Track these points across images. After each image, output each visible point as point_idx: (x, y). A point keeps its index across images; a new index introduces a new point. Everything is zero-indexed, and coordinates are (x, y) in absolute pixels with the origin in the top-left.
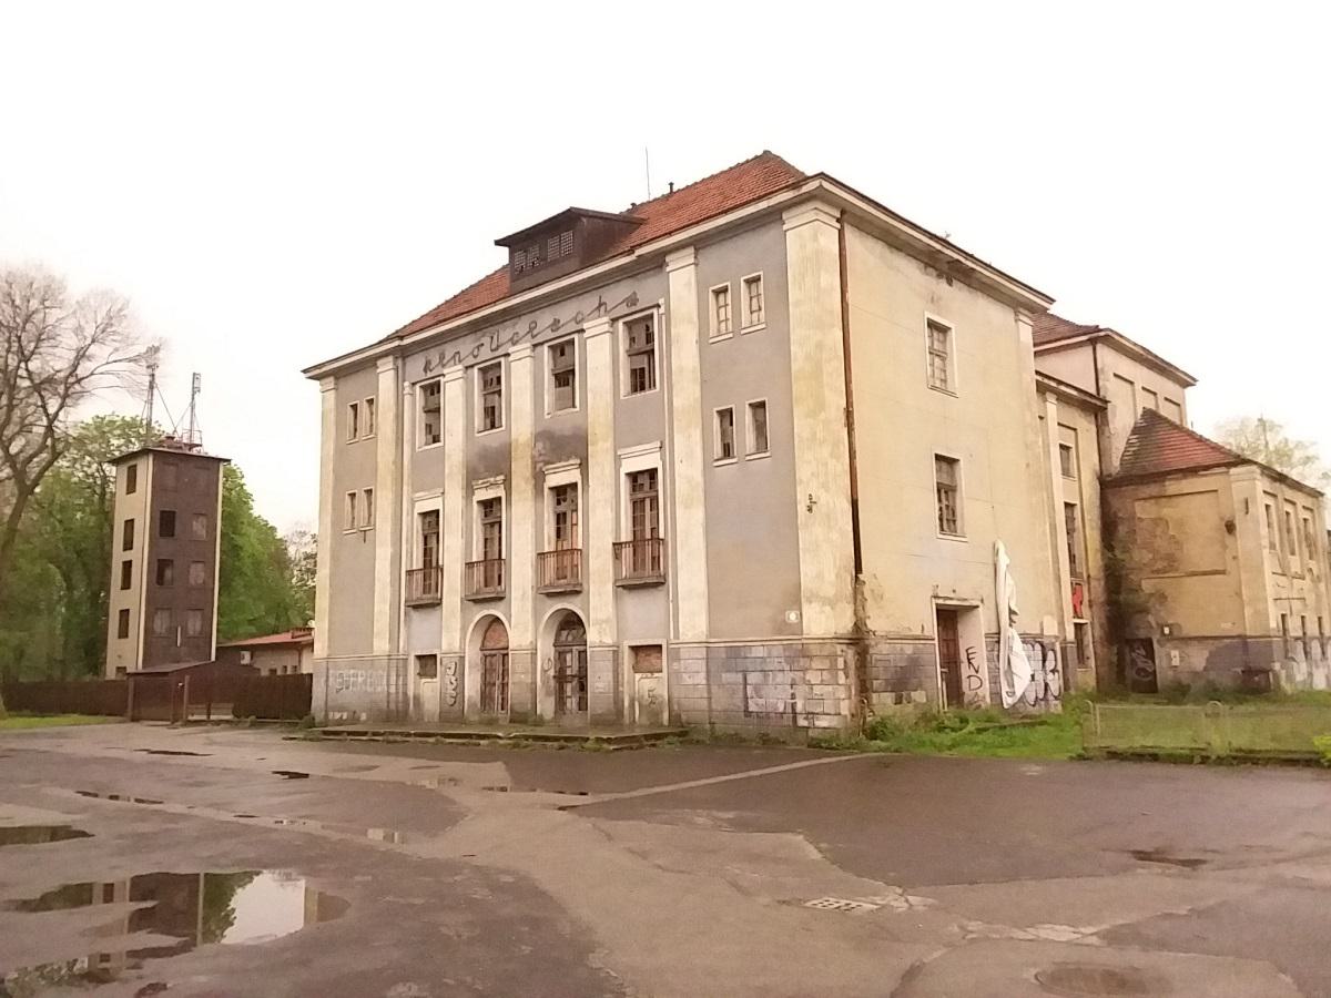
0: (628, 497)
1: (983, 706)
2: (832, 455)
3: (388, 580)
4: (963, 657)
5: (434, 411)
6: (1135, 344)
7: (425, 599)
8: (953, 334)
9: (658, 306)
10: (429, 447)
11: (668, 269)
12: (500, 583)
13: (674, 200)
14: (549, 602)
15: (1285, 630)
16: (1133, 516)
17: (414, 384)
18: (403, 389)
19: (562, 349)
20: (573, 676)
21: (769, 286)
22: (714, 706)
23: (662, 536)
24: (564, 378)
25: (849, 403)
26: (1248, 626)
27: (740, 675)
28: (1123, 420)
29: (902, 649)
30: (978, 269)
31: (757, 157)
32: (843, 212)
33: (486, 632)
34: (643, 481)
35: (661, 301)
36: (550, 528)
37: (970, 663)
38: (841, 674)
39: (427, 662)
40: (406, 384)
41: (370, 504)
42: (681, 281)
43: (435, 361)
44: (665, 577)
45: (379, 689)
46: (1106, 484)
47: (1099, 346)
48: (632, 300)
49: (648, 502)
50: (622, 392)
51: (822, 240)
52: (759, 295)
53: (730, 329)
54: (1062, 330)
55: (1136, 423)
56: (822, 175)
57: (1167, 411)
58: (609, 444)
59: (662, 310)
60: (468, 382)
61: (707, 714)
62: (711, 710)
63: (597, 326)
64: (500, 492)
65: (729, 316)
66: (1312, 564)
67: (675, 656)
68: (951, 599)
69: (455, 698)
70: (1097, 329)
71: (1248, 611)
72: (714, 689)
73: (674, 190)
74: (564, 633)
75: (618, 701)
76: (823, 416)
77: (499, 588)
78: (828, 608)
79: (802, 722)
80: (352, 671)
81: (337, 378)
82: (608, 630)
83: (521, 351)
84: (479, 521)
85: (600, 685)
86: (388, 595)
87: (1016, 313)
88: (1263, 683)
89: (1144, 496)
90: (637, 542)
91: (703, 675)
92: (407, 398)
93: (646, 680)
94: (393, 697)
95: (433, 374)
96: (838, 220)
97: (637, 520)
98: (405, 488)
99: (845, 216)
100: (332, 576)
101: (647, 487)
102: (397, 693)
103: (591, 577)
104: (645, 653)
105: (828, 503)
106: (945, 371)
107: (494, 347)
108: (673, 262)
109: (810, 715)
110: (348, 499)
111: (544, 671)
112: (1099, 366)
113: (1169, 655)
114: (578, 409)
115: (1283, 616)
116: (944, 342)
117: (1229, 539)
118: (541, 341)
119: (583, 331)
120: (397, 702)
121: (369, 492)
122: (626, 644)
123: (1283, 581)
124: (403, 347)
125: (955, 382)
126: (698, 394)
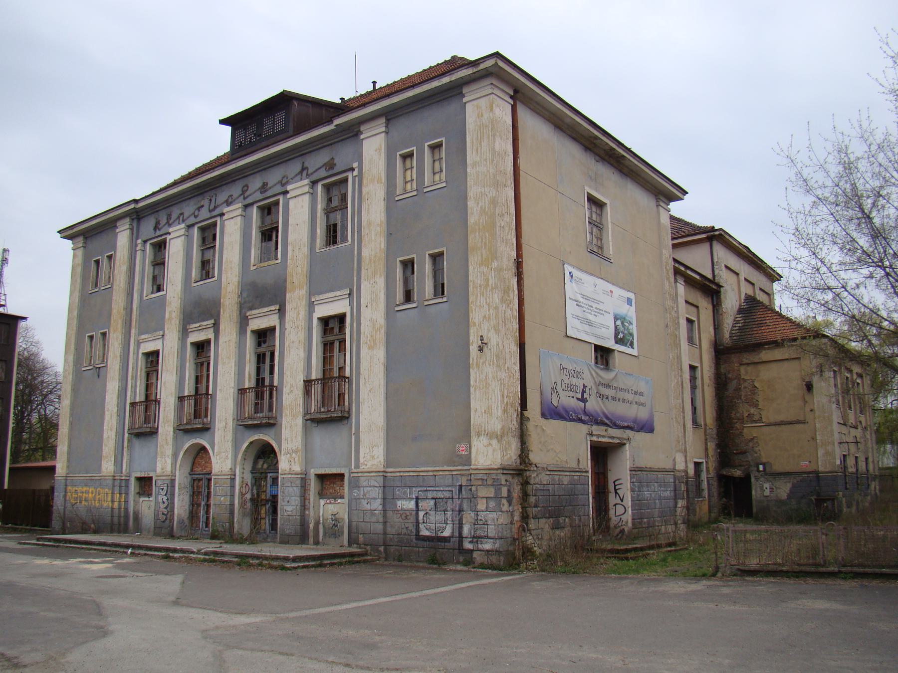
0: (320, 340)
1: (626, 530)
2: (502, 300)
3: (115, 410)
4: (611, 487)
5: (159, 263)
6: (740, 244)
7: (144, 431)
8: (608, 208)
9: (353, 169)
10: (153, 296)
11: (362, 137)
12: (206, 416)
13: (376, 95)
14: (247, 433)
15: (845, 467)
16: (738, 377)
17: (145, 242)
18: (136, 245)
19: (268, 210)
20: (267, 501)
21: (452, 148)
22: (389, 530)
23: (347, 374)
24: (269, 234)
25: (519, 255)
26: (820, 463)
27: (413, 503)
28: (731, 301)
29: (559, 480)
30: (631, 159)
31: (446, 61)
32: (516, 91)
33: (195, 459)
34: (333, 327)
35: (355, 165)
36: (250, 368)
37: (616, 493)
38: (504, 501)
39: (145, 484)
40: (139, 241)
41: (104, 345)
42: (374, 146)
43: (164, 221)
44: (349, 412)
45: (105, 505)
46: (721, 352)
47: (715, 243)
48: (330, 165)
49: (337, 345)
50: (318, 245)
51: (497, 111)
52: (441, 159)
53: (415, 187)
54: (686, 229)
55: (740, 305)
56: (497, 55)
57: (761, 297)
58: (303, 292)
59: (355, 173)
60: (188, 237)
61: (381, 536)
62: (385, 534)
63: (299, 188)
64: (210, 334)
65: (414, 177)
66: (862, 418)
67: (355, 484)
68: (603, 437)
69: (166, 515)
70: (712, 229)
71: (820, 452)
72: (390, 514)
73: (377, 87)
74: (261, 462)
75: (304, 523)
76: (495, 264)
77: (205, 420)
78: (494, 442)
79: (468, 545)
80: (85, 489)
81: (86, 238)
82: (297, 459)
83: (235, 209)
84: (192, 362)
85: (289, 508)
86: (114, 422)
87: (657, 200)
88: (830, 507)
89: (747, 361)
90: (326, 379)
91: (379, 501)
92: (139, 254)
93: (330, 506)
94: (116, 512)
95: (162, 232)
96: (511, 97)
97: (327, 360)
98: (133, 331)
99: (518, 95)
100: (73, 406)
101: (336, 330)
102: (120, 509)
103: (284, 411)
104: (330, 482)
105: (498, 345)
106: (601, 240)
107: (212, 207)
108: (367, 131)
109: (476, 539)
110: (87, 340)
111: (242, 495)
112: (715, 260)
113: (762, 488)
114: (279, 261)
115: (844, 456)
116: (600, 215)
117: (807, 398)
118: (251, 201)
119: (287, 192)
120: (119, 516)
121: (104, 334)
122: (313, 472)
123: (844, 430)
124: (137, 213)
125: (610, 249)
126: (383, 245)
